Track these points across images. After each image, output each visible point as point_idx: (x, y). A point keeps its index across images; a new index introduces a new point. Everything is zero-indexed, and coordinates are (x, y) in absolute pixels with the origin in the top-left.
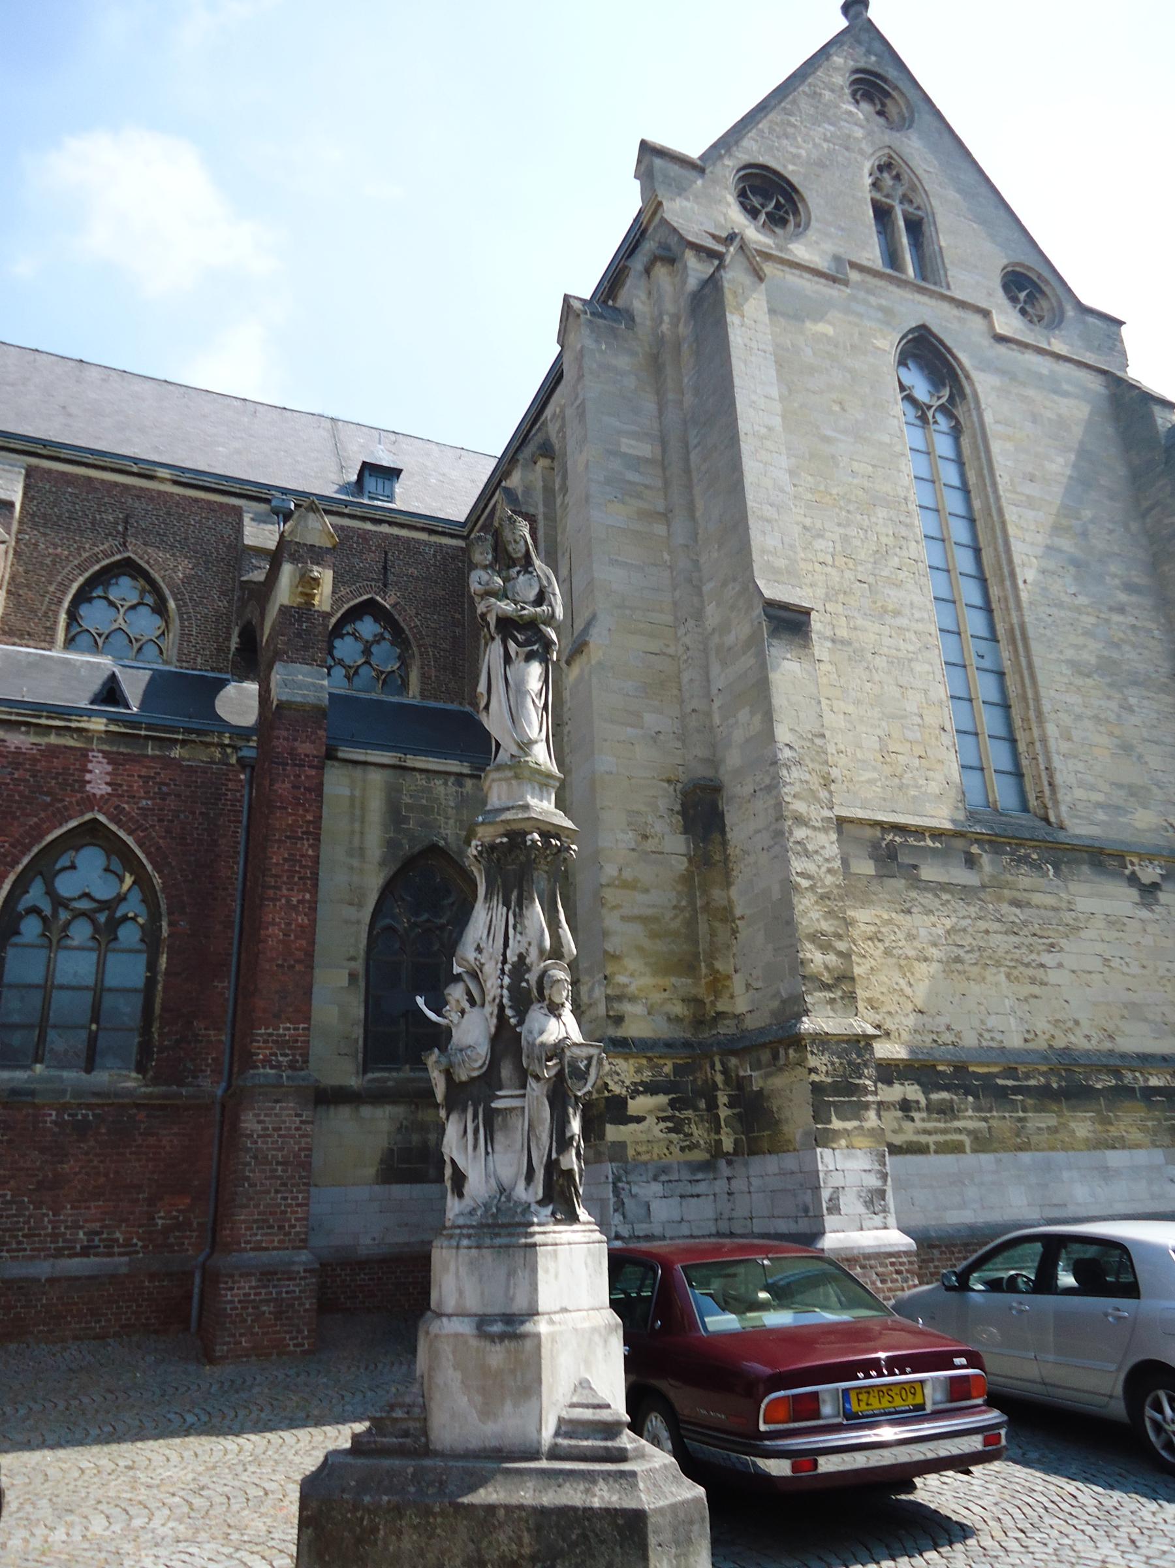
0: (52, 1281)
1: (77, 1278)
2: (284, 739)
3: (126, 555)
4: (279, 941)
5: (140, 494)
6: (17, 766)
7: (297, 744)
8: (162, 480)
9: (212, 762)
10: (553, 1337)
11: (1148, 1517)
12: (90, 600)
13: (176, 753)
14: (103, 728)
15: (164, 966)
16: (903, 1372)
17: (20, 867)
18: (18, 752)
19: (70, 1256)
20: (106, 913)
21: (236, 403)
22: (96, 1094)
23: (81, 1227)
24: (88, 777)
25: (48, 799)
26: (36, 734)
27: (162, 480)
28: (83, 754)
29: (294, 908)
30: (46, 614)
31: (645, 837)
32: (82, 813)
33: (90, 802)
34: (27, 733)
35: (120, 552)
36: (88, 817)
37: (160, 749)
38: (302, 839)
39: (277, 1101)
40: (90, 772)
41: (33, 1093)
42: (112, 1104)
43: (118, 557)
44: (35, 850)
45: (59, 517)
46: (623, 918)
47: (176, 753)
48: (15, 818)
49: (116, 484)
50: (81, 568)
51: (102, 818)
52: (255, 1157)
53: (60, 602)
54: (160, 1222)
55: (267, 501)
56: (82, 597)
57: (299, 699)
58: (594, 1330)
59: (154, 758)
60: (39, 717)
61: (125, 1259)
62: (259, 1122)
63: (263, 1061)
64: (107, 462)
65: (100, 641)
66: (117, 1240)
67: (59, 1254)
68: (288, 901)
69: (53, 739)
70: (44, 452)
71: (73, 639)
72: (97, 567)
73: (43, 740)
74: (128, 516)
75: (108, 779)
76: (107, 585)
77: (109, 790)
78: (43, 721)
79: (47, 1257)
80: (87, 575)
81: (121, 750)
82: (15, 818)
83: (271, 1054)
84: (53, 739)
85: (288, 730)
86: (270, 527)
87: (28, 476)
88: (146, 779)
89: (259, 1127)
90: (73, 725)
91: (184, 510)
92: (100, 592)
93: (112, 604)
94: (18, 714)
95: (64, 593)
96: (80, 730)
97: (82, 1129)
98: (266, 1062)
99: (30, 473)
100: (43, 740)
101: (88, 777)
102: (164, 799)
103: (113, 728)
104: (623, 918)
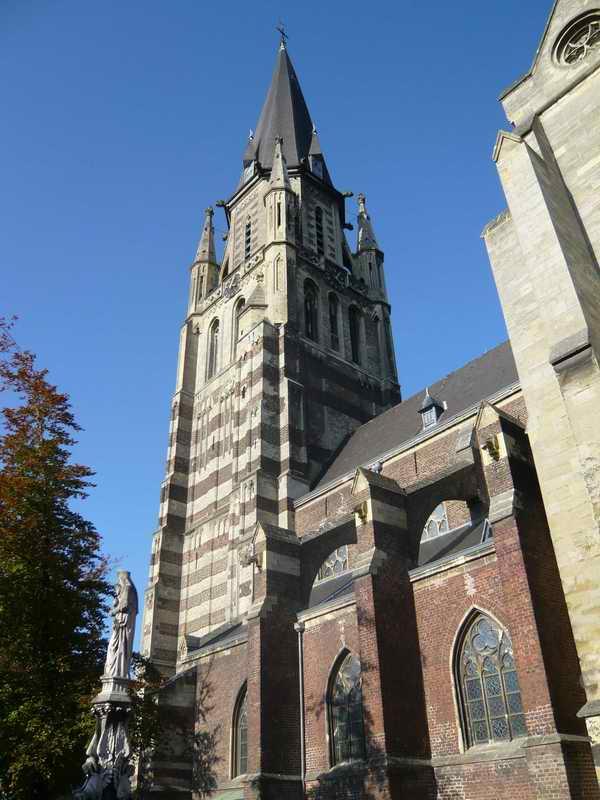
4: (525, 658)
6: (441, 594)
11: (38, 496)
17: (454, 643)
29: (526, 636)
31: (588, 548)
33: (470, 600)
36: (471, 608)
39: (543, 754)
46: (583, 613)
51: (477, 607)
52: (539, 788)
78: (443, 569)
88: (487, 578)
89: (537, 770)
97: (507, 772)
104: (583, 613)
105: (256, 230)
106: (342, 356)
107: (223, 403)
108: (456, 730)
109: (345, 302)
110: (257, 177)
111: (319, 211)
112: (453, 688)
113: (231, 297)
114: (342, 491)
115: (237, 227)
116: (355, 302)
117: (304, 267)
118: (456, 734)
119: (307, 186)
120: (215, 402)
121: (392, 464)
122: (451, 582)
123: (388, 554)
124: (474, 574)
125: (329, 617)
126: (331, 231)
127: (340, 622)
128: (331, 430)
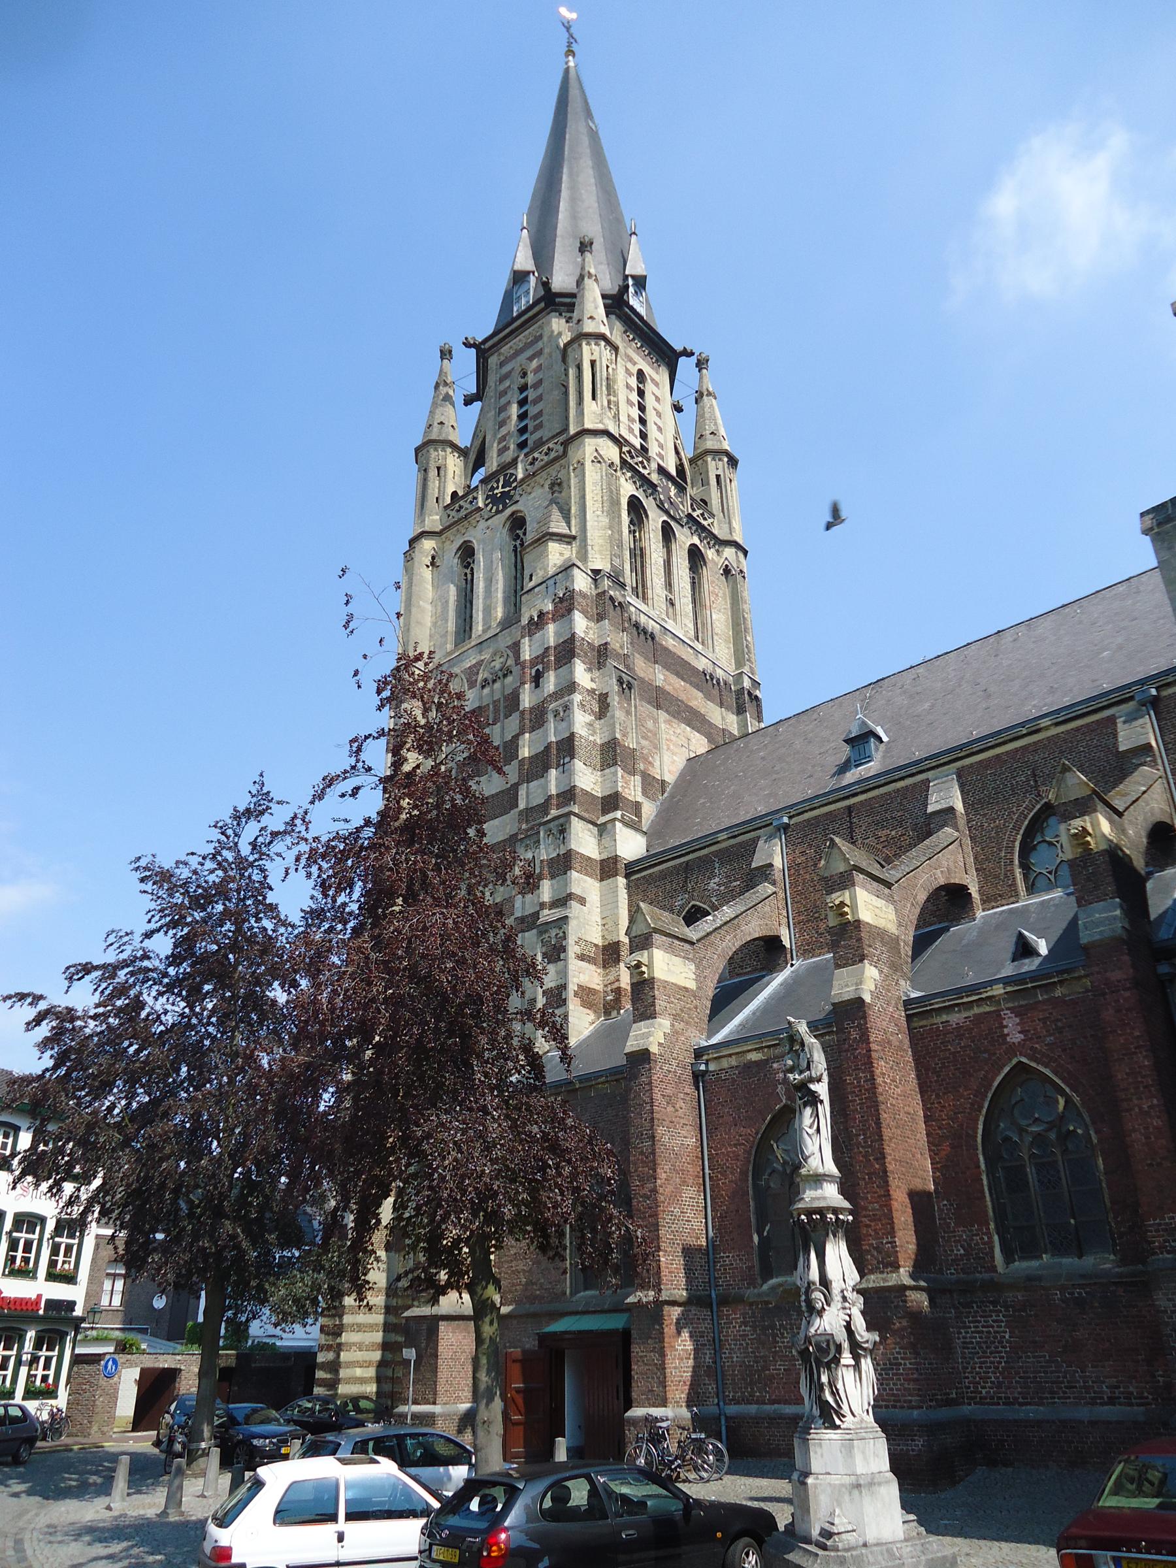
0: (1093, 1423)
1: (1109, 1423)
2: (1098, 973)
3: (1043, 802)
5: (1035, 748)
6: (960, 1037)
7: (1108, 974)
8: (1047, 728)
9: (1087, 991)
10: (815, 1486)
12: (1034, 848)
13: (1058, 992)
14: (1002, 991)
15: (1102, 1167)
16: (1129, 1551)
17: (984, 1111)
18: (959, 1027)
19: (1102, 1404)
20: (1055, 1130)
21: (1121, 588)
22: (1083, 1276)
23: (1104, 1382)
24: (1006, 1031)
25: (986, 1055)
26: (965, 1010)
27: (1047, 728)
28: (997, 1013)
30: (1006, 876)
32: (1011, 1060)
33: (1012, 1050)
34: (960, 1011)
35: (1038, 802)
36: (1015, 1061)
37: (1047, 993)
38: (1135, 1053)
40: (1006, 1027)
41: (1039, 1278)
42: (1095, 1284)
43: (1038, 807)
44: (990, 1095)
45: (989, 797)
47: (1058, 992)
48: (971, 1075)
49: (1017, 750)
50: (1016, 828)
51: (1024, 1060)
53: (1012, 862)
54: (1161, 1379)
55: (1132, 698)
56: (1027, 849)
57: (1097, 937)
58: (842, 1485)
59: (1044, 1002)
60: (962, 998)
61: (1142, 1408)
62: (1169, 1300)
63: (1160, 1248)
64: (1004, 737)
65: (1052, 877)
66: (1132, 1393)
67: (1093, 1402)
68: (1141, 1109)
69: (976, 1010)
70: (963, 754)
71: (1033, 884)
72: (1026, 823)
73: (970, 1013)
74: (1033, 772)
75: (1019, 1028)
76: (1042, 830)
77: (1022, 1036)
78: (965, 1000)
79: (1087, 1404)
80: (1022, 832)
81: (1022, 1003)
82: (971, 1075)
83: (1165, 1241)
84: (976, 1010)
85: (1098, 965)
86: (1141, 721)
87: (959, 777)
88: (1044, 1020)
90: (983, 996)
91: (1071, 742)
92: (1039, 838)
93: (1050, 844)
94: (949, 1000)
95: (1012, 853)
96: (989, 998)
98: (1162, 1248)
99: (962, 777)
100: (970, 1013)
101: (1006, 1031)
102: (1061, 1033)
103: (1009, 989)
105: (539, 399)
106: (683, 627)
107: (486, 691)
108: (990, 1238)
109: (685, 538)
110: (558, 300)
111: (641, 375)
112: (984, 1177)
113: (498, 512)
114: (714, 853)
115: (502, 388)
116: (696, 540)
117: (629, 474)
118: (991, 1241)
119: (625, 332)
120: (472, 685)
121: (808, 820)
122: (978, 1019)
123: (881, 972)
124: (1018, 1012)
125: (754, 1056)
126: (659, 415)
127: (775, 1065)
128: (668, 749)
